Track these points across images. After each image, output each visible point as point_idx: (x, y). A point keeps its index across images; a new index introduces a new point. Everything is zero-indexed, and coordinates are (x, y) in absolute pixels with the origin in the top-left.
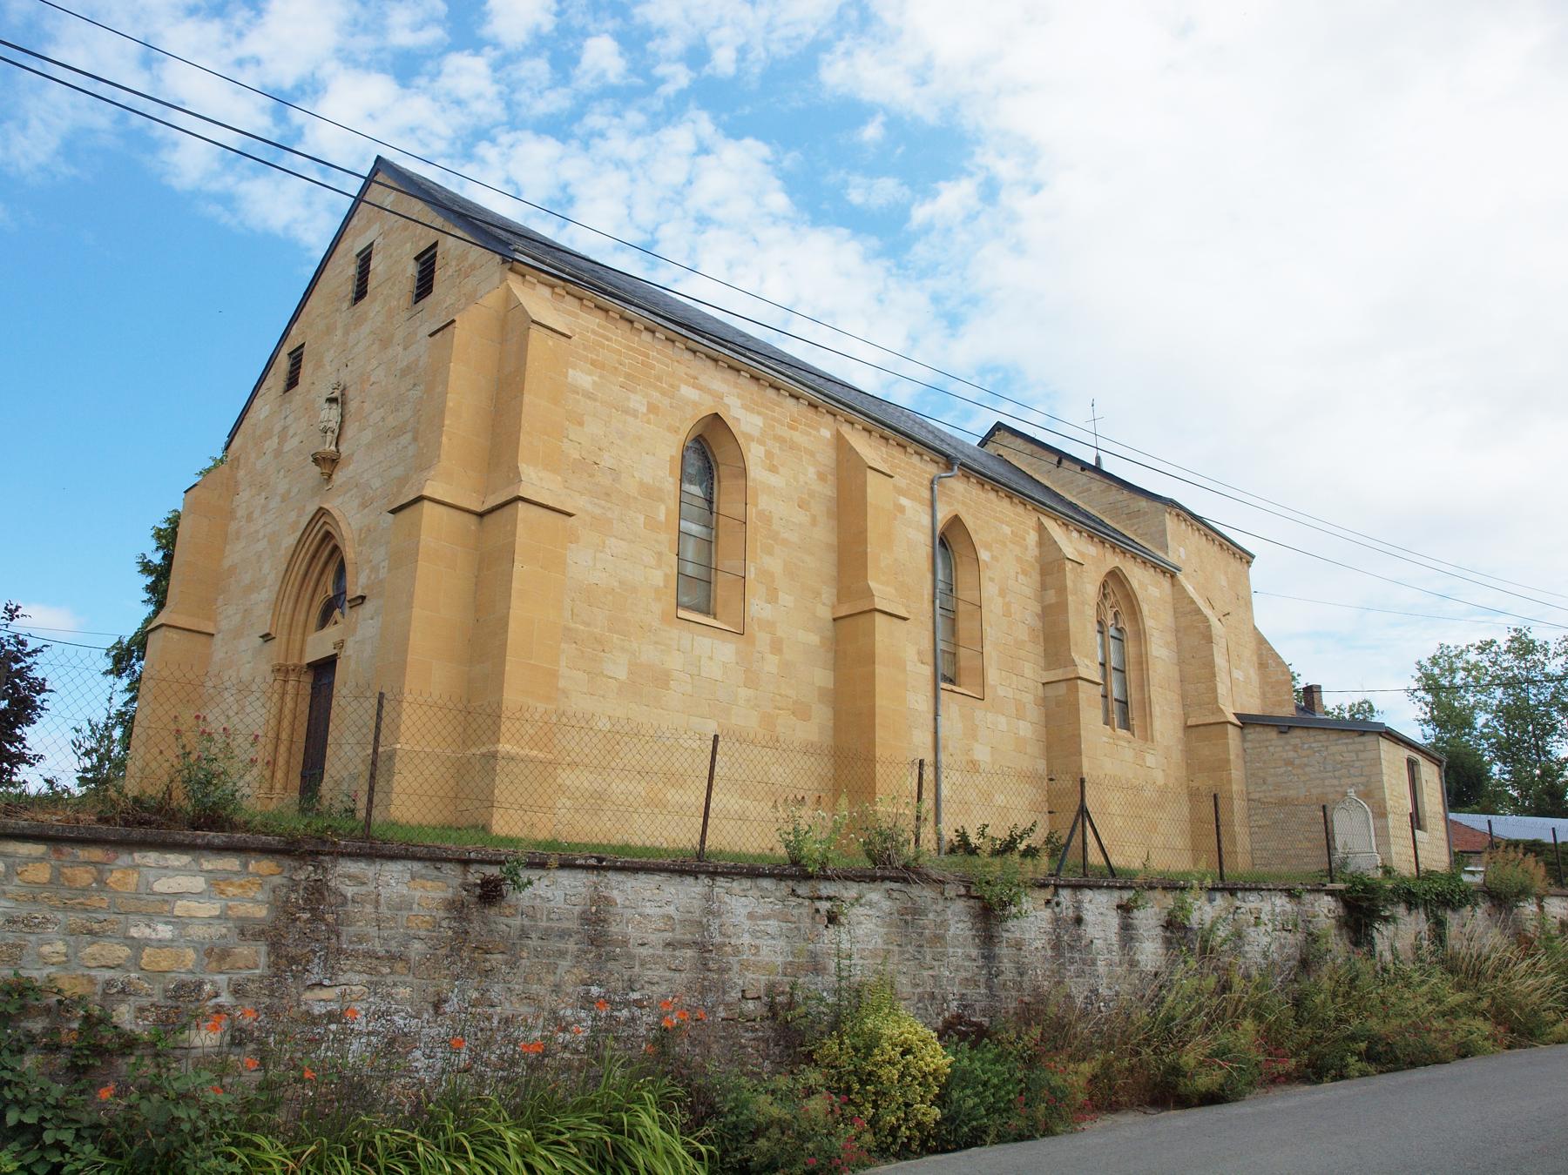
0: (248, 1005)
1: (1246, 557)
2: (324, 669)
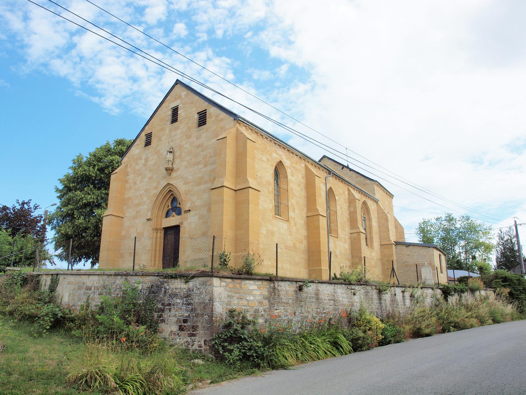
0: (266, 313)
1: (391, 196)
2: (176, 229)
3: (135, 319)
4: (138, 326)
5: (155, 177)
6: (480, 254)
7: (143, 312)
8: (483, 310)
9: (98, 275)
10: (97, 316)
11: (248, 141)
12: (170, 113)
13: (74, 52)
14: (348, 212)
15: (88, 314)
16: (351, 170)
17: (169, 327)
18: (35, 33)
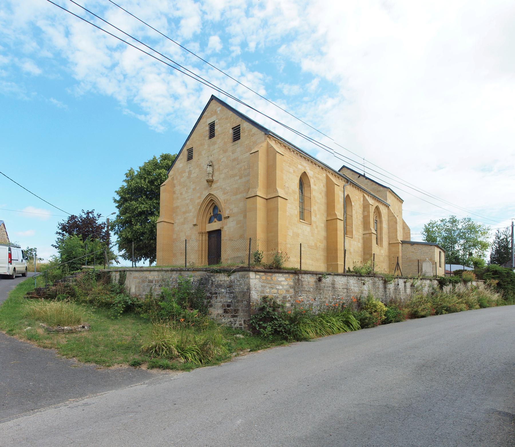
1: (402, 201)
2: (218, 233)
3: (189, 305)
4: (192, 310)
5: (198, 188)
6: (477, 251)
7: (195, 299)
8: (473, 298)
9: (158, 271)
10: (160, 303)
11: (278, 155)
12: (208, 128)
13: (117, 70)
14: (362, 216)
15: (152, 302)
16: (367, 178)
17: (216, 311)
18: (78, 50)
